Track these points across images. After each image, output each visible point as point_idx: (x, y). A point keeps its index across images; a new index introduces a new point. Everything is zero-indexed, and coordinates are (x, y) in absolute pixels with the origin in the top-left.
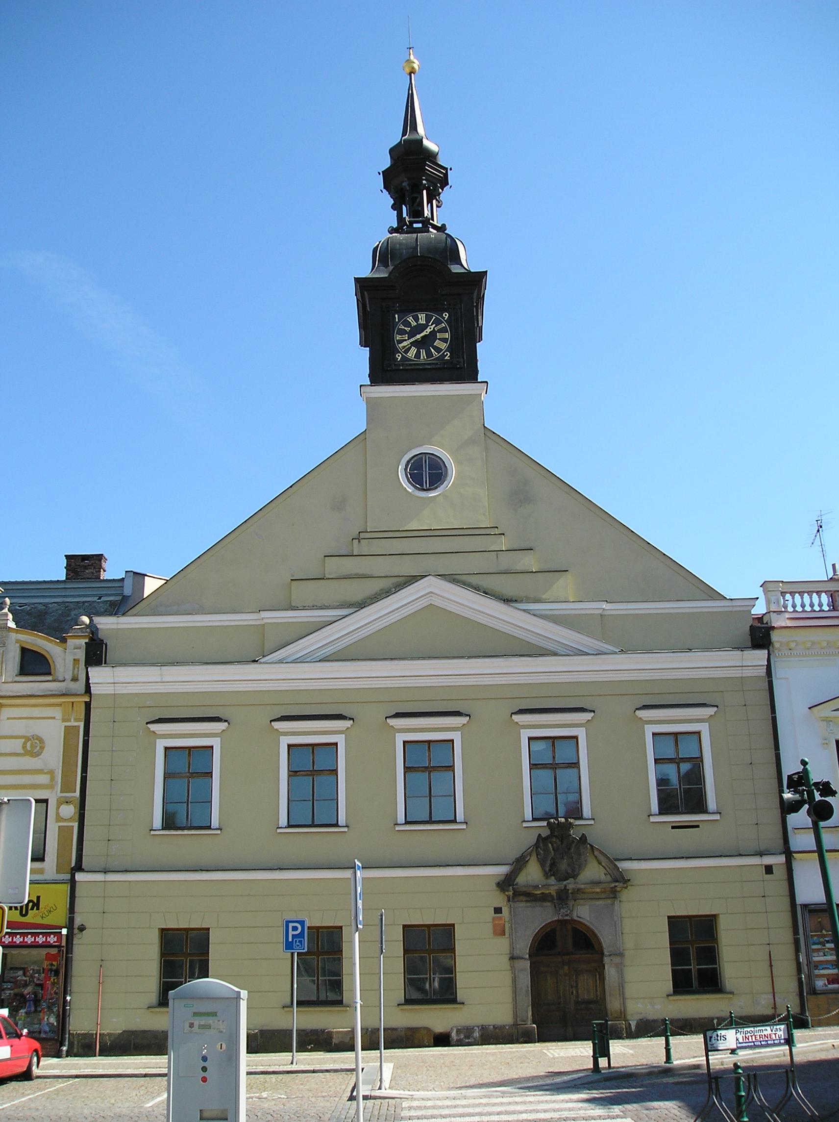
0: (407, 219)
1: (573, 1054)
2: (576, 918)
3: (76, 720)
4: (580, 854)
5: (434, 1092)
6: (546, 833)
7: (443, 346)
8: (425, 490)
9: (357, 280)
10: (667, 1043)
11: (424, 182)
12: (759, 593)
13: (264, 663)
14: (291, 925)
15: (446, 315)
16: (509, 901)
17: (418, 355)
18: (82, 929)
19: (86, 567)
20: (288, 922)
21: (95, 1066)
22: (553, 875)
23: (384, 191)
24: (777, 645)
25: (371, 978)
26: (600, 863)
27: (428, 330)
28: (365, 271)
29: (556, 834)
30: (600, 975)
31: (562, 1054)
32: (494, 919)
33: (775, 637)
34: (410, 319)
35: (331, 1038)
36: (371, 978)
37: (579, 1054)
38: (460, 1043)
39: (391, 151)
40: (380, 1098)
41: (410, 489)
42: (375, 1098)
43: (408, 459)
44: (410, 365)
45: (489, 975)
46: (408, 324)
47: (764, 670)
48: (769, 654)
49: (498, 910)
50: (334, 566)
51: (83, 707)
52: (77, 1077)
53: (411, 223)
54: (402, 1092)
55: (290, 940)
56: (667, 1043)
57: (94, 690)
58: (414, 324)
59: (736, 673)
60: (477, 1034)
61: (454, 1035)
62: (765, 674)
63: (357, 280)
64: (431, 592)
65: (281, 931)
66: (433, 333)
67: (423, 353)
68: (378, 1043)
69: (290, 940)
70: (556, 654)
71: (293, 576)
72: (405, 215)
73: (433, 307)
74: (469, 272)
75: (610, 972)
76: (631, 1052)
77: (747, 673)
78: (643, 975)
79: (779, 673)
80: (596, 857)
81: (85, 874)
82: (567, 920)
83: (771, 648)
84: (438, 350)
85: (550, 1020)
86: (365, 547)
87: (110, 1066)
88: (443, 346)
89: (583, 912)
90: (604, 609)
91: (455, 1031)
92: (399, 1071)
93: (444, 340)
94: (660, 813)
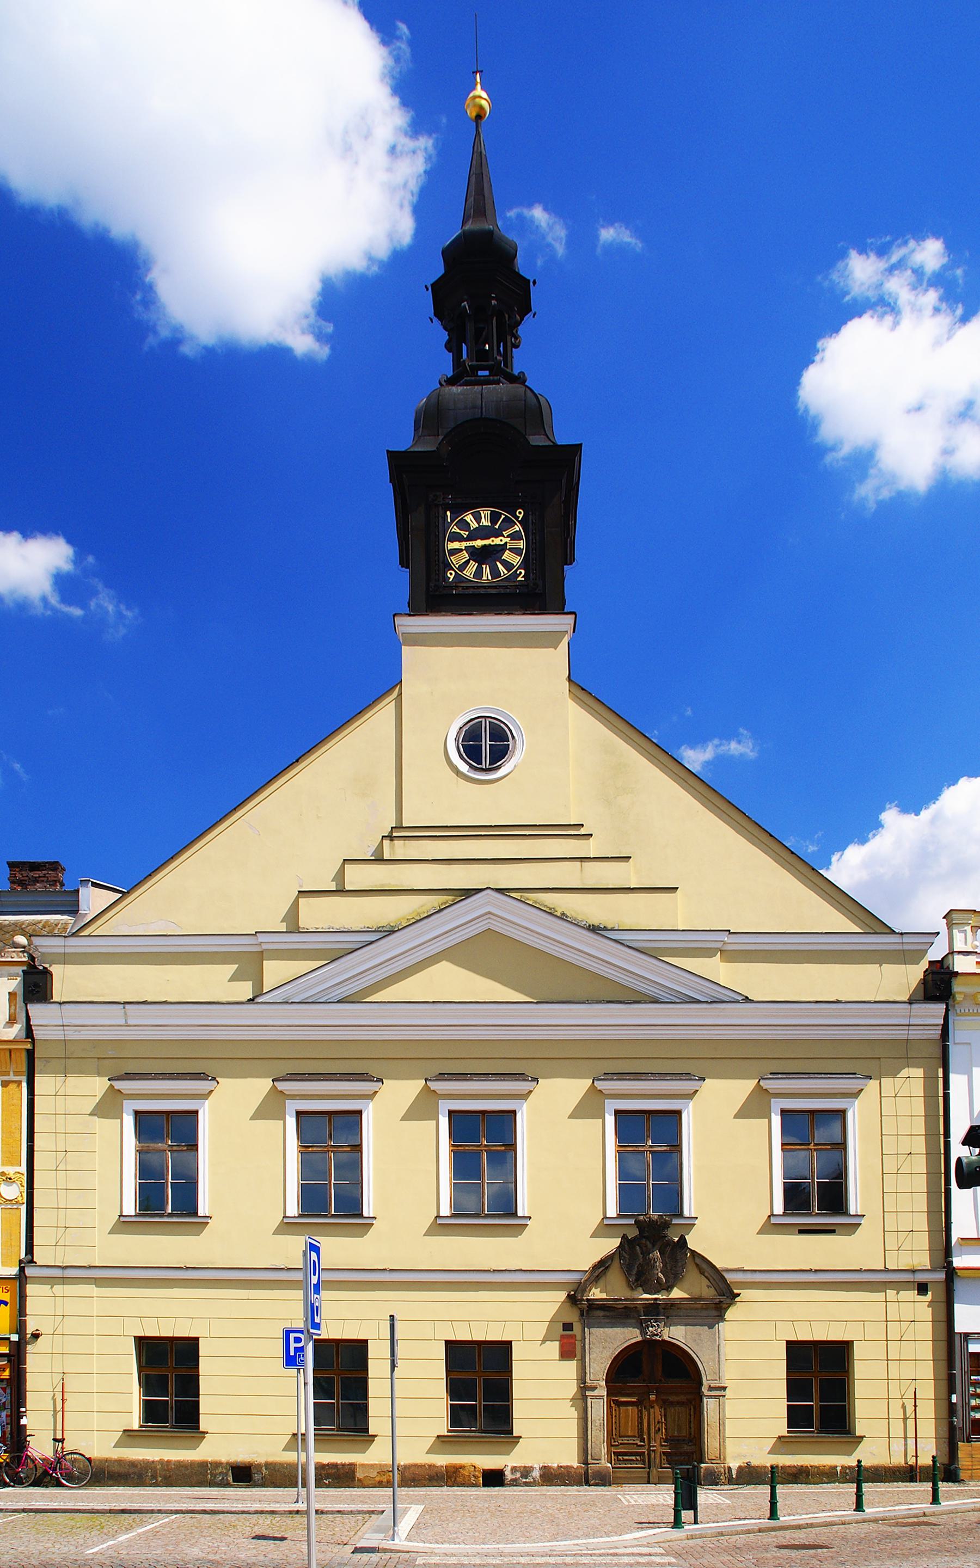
0: (468, 363)
1: (654, 1501)
2: (666, 1338)
3: (16, 1073)
4: (676, 1261)
5: (463, 1546)
6: (633, 1233)
7: (516, 560)
8: (482, 770)
9: (392, 455)
10: (859, 1489)
11: (493, 302)
12: (942, 926)
13: (262, 1003)
14: (292, 1336)
15: (520, 514)
16: (582, 1315)
17: (479, 573)
18: (36, 1336)
19: (36, 880)
20: (288, 1333)
21: (116, 1497)
22: (641, 1286)
23: (435, 319)
24: (959, 998)
25: (411, 1408)
26: (702, 1273)
27: (497, 541)
28: (404, 441)
29: (646, 1234)
30: (694, 1408)
31: (640, 1502)
32: (562, 1336)
33: (958, 987)
34: (469, 518)
35: (354, 1472)
36: (411, 1408)
37: (662, 1501)
38: (515, 1483)
39: (445, 253)
40: (391, 1551)
41: (464, 767)
42: (385, 1551)
43: (461, 724)
44: (468, 588)
45: (551, 1407)
46: (464, 525)
47: (938, 1032)
48: (947, 1010)
49: (568, 1327)
50: (356, 877)
51: (24, 1056)
52: (24, 1511)
53: (474, 369)
54: (421, 1545)
55: (292, 1353)
56: (859, 1489)
57: (38, 1034)
58: (474, 525)
59: (900, 1034)
60: (536, 1474)
61: (508, 1473)
62: (938, 1037)
63: (392, 455)
64: (489, 913)
65: (280, 1344)
66: (503, 548)
67: (486, 570)
68: (297, 1482)
69: (292, 1353)
70: (656, 1001)
71: (301, 886)
72: (465, 356)
73: (502, 501)
74: (555, 446)
75: (709, 1405)
76: (728, 1502)
77: (914, 1034)
78: (748, 1412)
79: (958, 1034)
80: (697, 1265)
81: (38, 1268)
82: (656, 1340)
83: (950, 1002)
84: (508, 566)
85: (626, 1460)
86: (401, 849)
87: (131, 1498)
88: (516, 560)
89: (677, 1334)
90: (725, 943)
91: (509, 1468)
92: (427, 1517)
93: (517, 551)
94: (785, 1214)
